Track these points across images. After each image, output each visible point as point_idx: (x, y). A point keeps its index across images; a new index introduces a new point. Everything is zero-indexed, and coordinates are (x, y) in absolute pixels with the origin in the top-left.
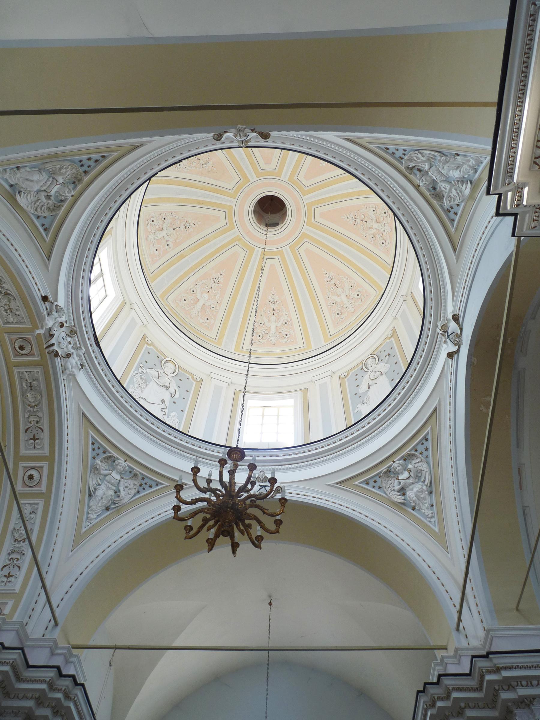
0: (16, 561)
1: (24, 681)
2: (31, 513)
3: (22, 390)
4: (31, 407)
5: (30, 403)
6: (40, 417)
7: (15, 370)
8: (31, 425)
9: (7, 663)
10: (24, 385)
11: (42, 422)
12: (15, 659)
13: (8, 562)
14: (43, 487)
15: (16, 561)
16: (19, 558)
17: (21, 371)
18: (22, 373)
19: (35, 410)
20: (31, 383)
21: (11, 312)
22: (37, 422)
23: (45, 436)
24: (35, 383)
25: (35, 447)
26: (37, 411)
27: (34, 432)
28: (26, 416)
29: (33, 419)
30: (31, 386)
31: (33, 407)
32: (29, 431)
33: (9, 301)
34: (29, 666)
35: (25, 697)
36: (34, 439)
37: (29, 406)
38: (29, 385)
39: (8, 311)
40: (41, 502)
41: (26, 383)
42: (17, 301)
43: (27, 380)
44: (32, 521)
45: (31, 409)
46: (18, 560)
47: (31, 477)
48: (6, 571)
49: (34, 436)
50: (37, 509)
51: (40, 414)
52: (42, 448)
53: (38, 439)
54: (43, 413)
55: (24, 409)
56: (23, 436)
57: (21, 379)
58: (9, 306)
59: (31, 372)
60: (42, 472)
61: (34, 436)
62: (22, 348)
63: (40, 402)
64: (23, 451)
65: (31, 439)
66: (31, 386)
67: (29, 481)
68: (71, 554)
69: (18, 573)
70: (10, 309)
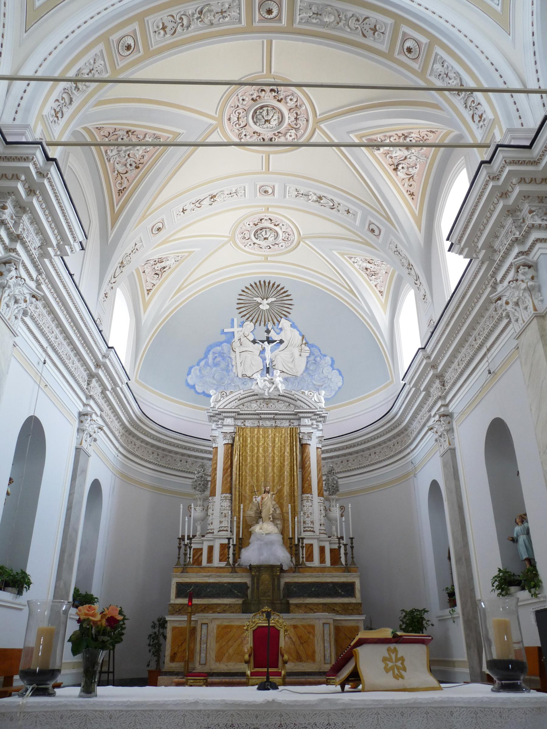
0: (474, 103)
1: (541, 159)
2: (443, 66)
3: (320, 25)
4: (340, 21)
5: (336, 22)
6: (353, 15)
7: (296, 25)
8: (360, 28)
9: (504, 167)
10: (314, 21)
11: (358, 15)
12: (503, 158)
13: (471, 112)
14: (424, 40)
15: (474, 103)
16: (473, 99)
17: (298, 20)
18: (301, 19)
19: (344, 18)
20: (314, 13)
21: (225, 12)
22: (358, 20)
23: (375, 16)
24: (314, 9)
25: (383, 33)
26: (345, 16)
27: (367, 27)
28: (349, 30)
29: (352, 23)
30: (317, 14)
31: (341, 20)
32: (365, 32)
33: (210, 11)
34: (530, 147)
35: (502, 171)
36: (374, 30)
37: (338, 23)
38: (315, 16)
39: (225, 15)
40: (438, 50)
41: (313, 18)
42: (211, 3)
43: (310, 17)
44: (450, 68)
45: (343, 22)
46: (473, 101)
47: (409, 50)
48: (477, 118)
49: (371, 29)
50: (441, 58)
51: (349, 14)
52: (386, 25)
53: (375, 26)
54: (349, 11)
55: (342, 29)
56: (369, 42)
57: (307, 22)
58: (217, 13)
59: (300, 9)
60: (409, 35)
61: (371, 29)
62: (270, 12)
63: (336, 10)
64: (384, 48)
65: (374, 34)
66: (317, 14)
67: (412, 54)
68: (511, 37)
69: (482, 108)
70: (222, 12)
